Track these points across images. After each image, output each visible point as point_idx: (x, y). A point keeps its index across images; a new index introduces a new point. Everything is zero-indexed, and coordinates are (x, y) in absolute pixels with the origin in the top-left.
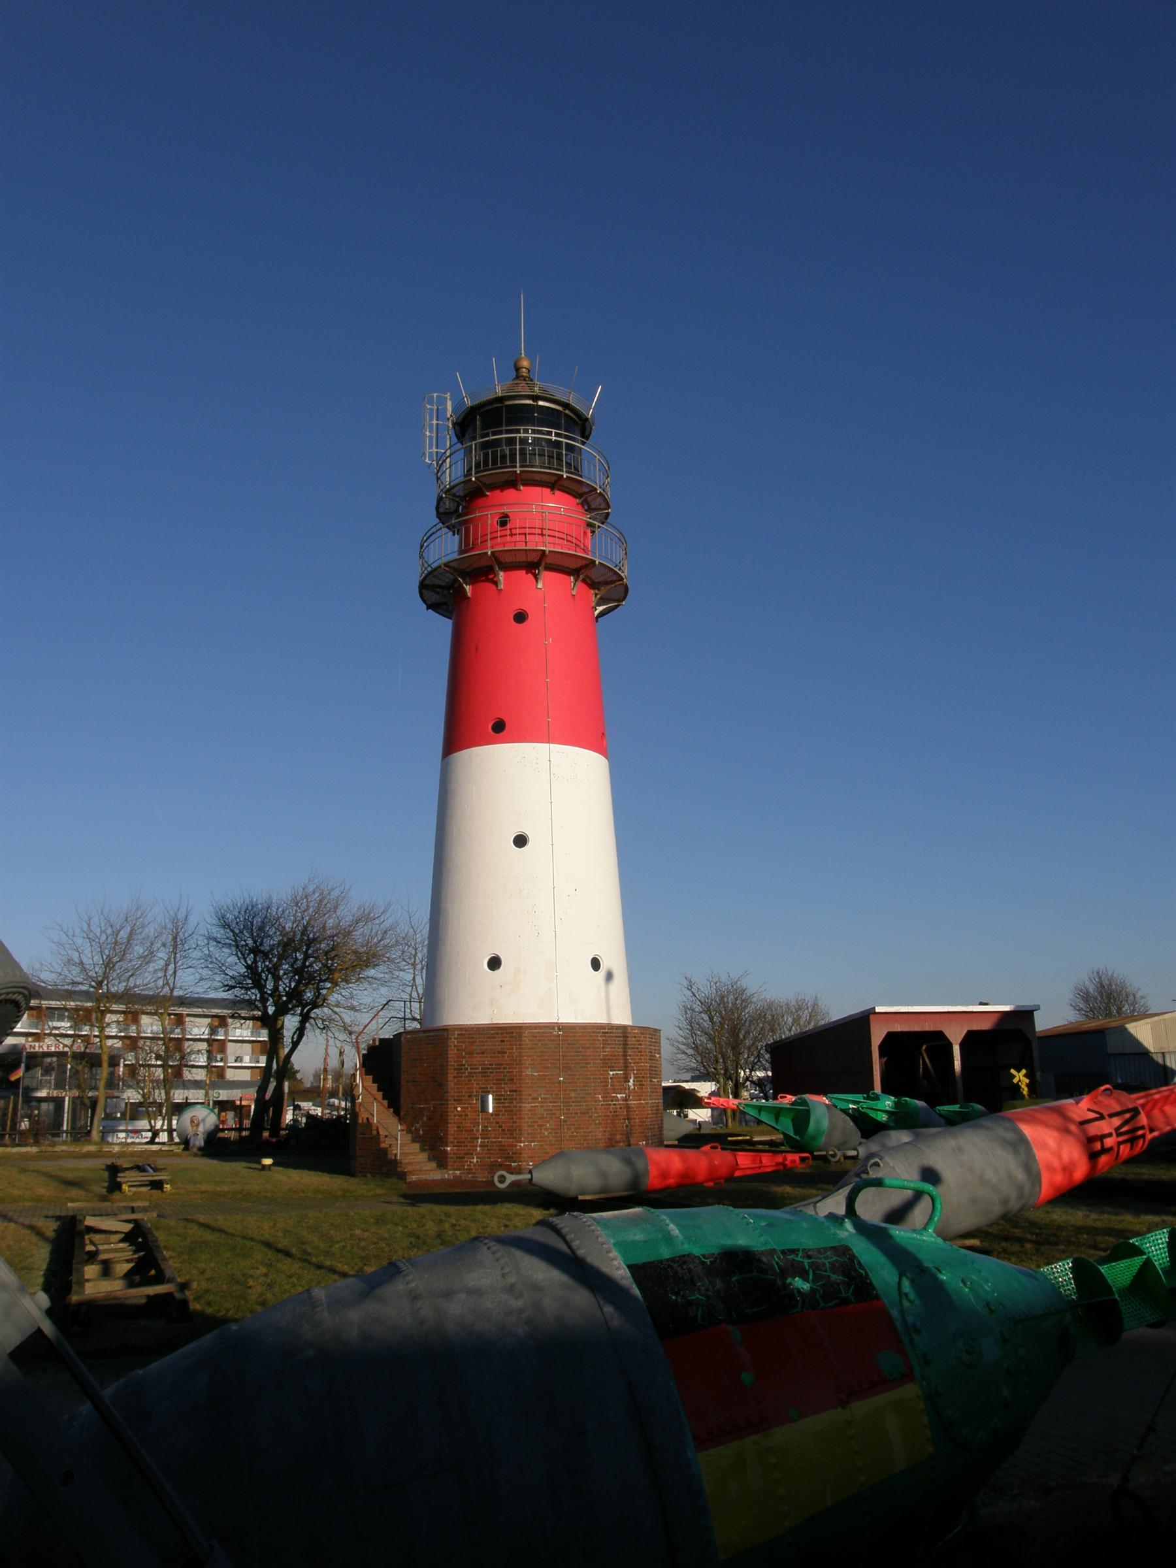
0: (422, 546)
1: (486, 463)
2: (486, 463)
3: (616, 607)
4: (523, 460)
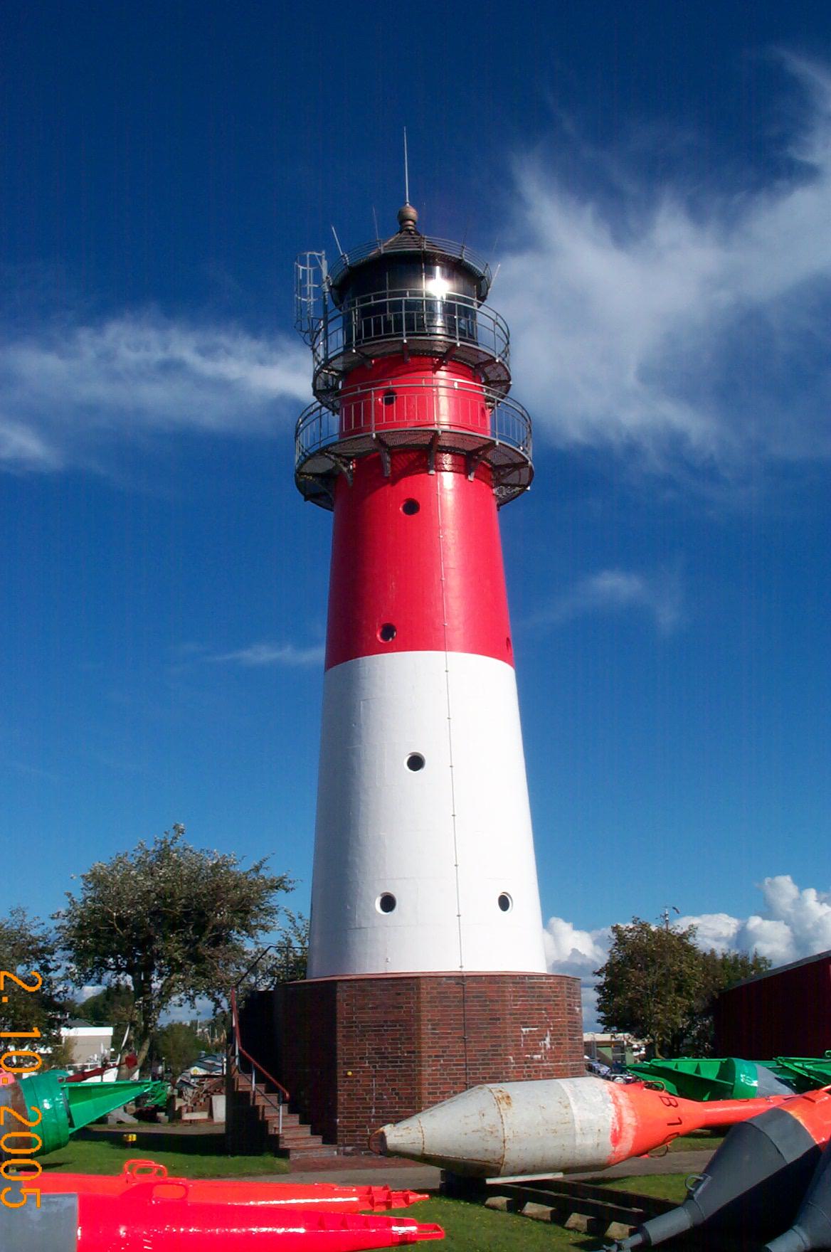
0: (297, 429)
1: (368, 333)
2: (368, 333)
3: (521, 492)
4: (410, 327)
